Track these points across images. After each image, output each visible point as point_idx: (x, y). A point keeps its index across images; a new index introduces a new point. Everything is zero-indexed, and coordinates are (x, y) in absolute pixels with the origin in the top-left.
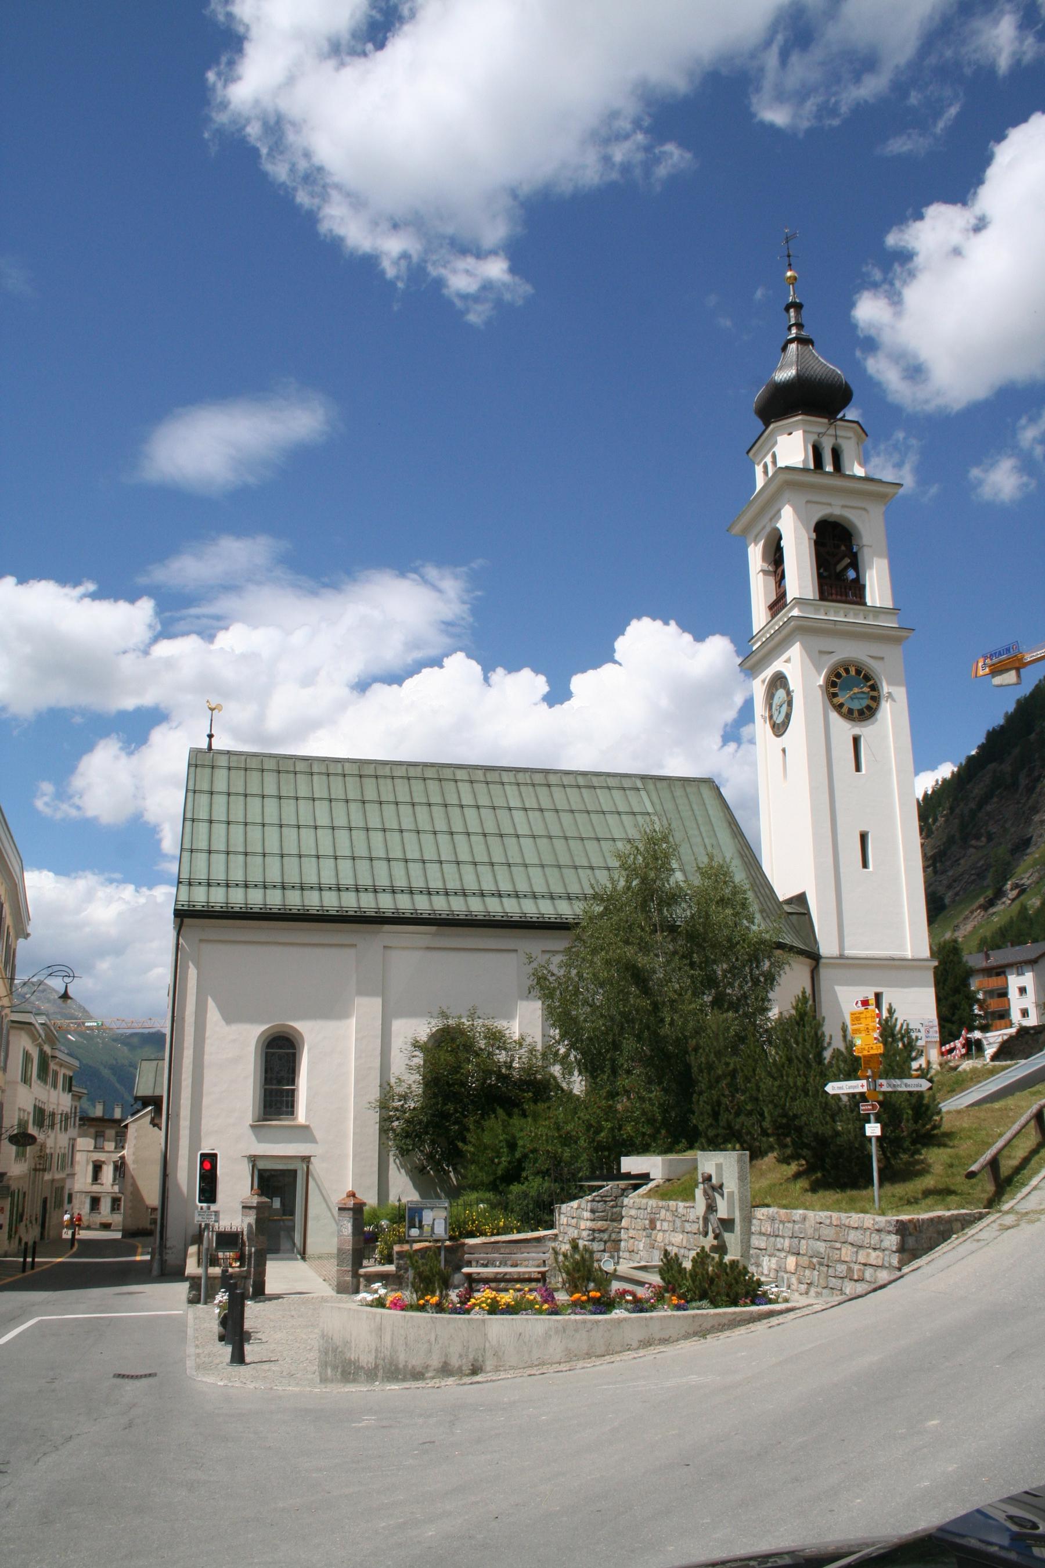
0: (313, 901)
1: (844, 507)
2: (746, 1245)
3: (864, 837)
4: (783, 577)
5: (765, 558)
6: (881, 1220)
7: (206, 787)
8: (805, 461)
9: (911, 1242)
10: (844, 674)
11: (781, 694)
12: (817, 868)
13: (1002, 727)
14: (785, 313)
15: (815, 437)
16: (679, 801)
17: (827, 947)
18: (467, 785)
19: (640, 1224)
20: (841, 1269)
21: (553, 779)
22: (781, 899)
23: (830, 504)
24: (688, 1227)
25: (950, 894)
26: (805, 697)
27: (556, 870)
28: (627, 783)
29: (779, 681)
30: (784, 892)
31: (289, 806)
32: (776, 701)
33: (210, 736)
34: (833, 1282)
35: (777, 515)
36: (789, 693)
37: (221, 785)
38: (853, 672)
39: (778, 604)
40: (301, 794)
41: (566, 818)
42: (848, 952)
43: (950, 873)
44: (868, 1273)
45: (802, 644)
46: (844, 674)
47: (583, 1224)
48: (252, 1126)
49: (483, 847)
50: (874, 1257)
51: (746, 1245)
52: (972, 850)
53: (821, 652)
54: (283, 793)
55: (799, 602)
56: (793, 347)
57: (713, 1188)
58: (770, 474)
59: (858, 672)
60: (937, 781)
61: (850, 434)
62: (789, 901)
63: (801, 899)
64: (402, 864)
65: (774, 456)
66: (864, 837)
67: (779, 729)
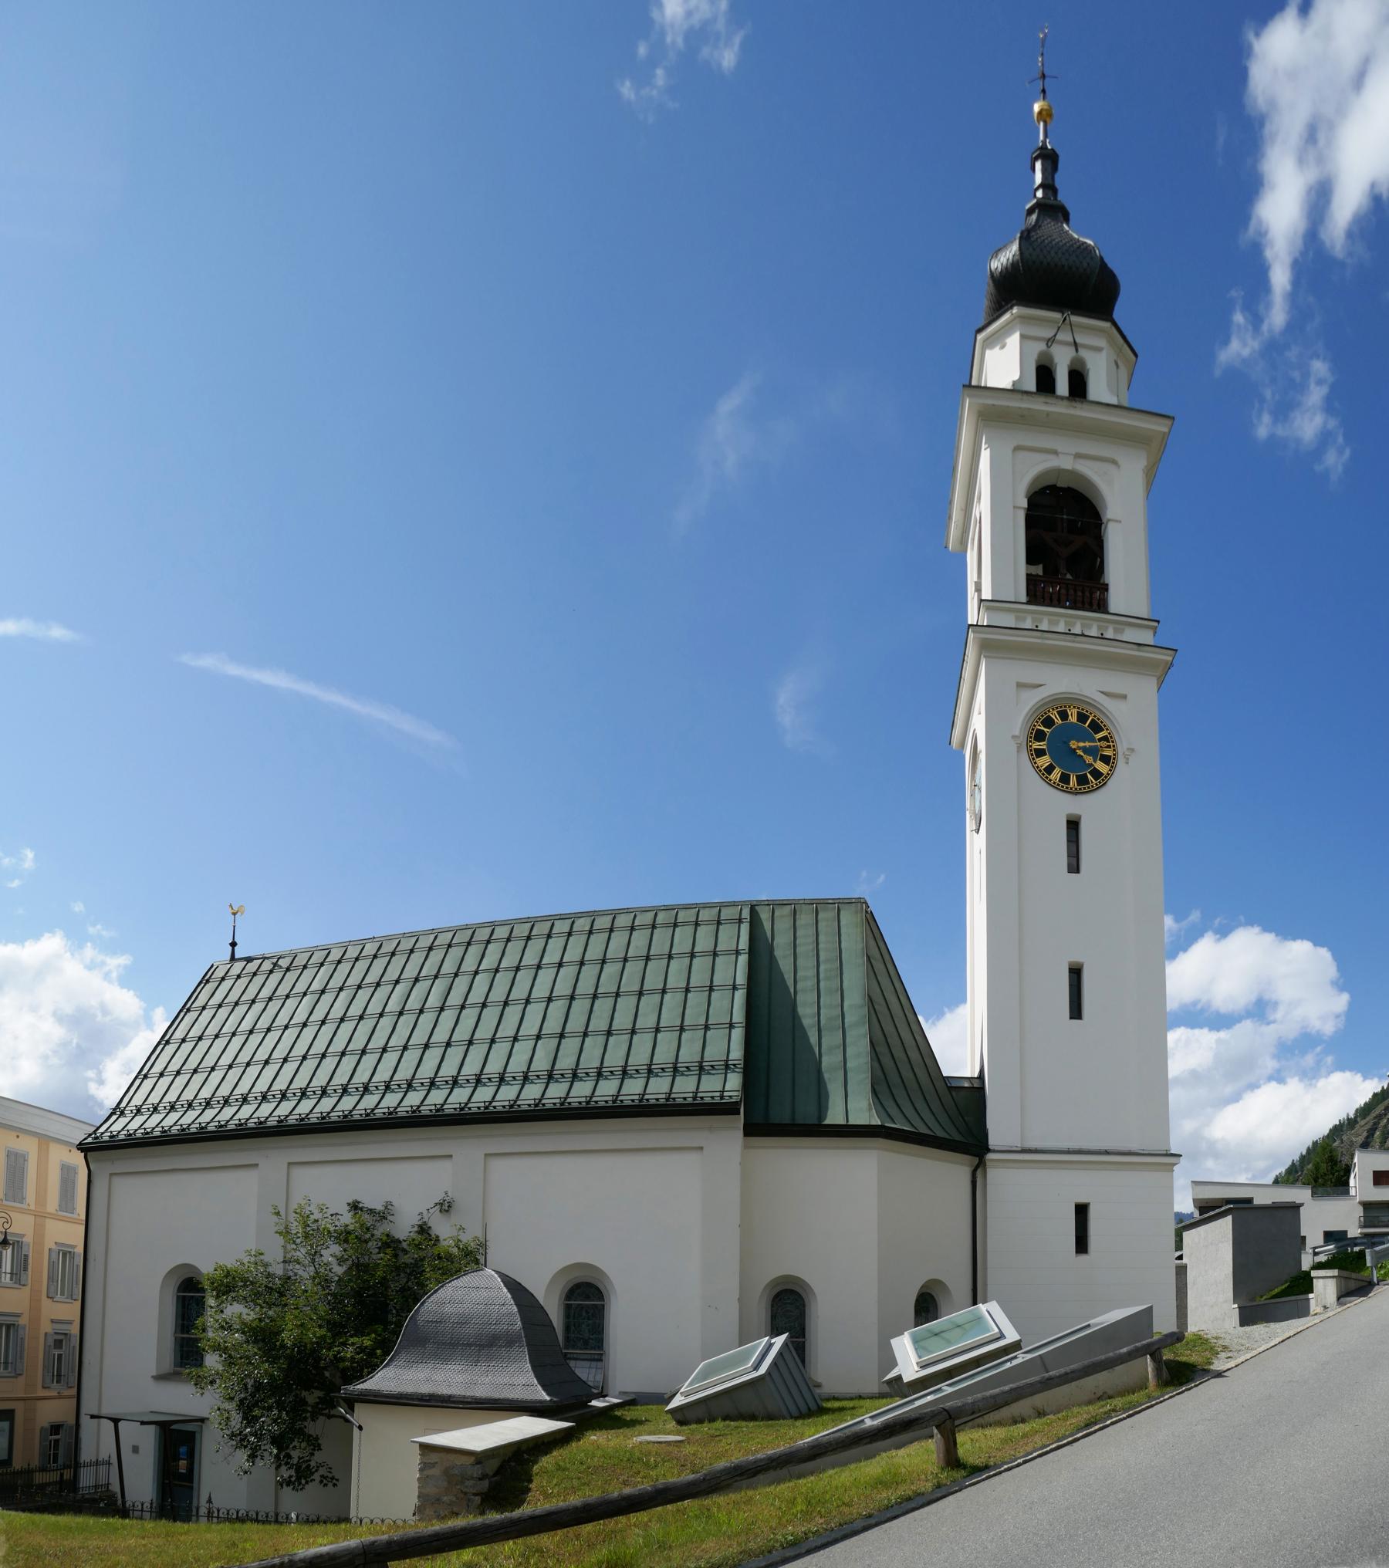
1: (1078, 456)
10: (1058, 721)
14: (982, 294)
15: (1042, 346)
23: (1056, 453)
33: (233, 944)
38: (1073, 718)
46: (1058, 721)
53: (1021, 686)
59: (1082, 717)
61: (1102, 342)
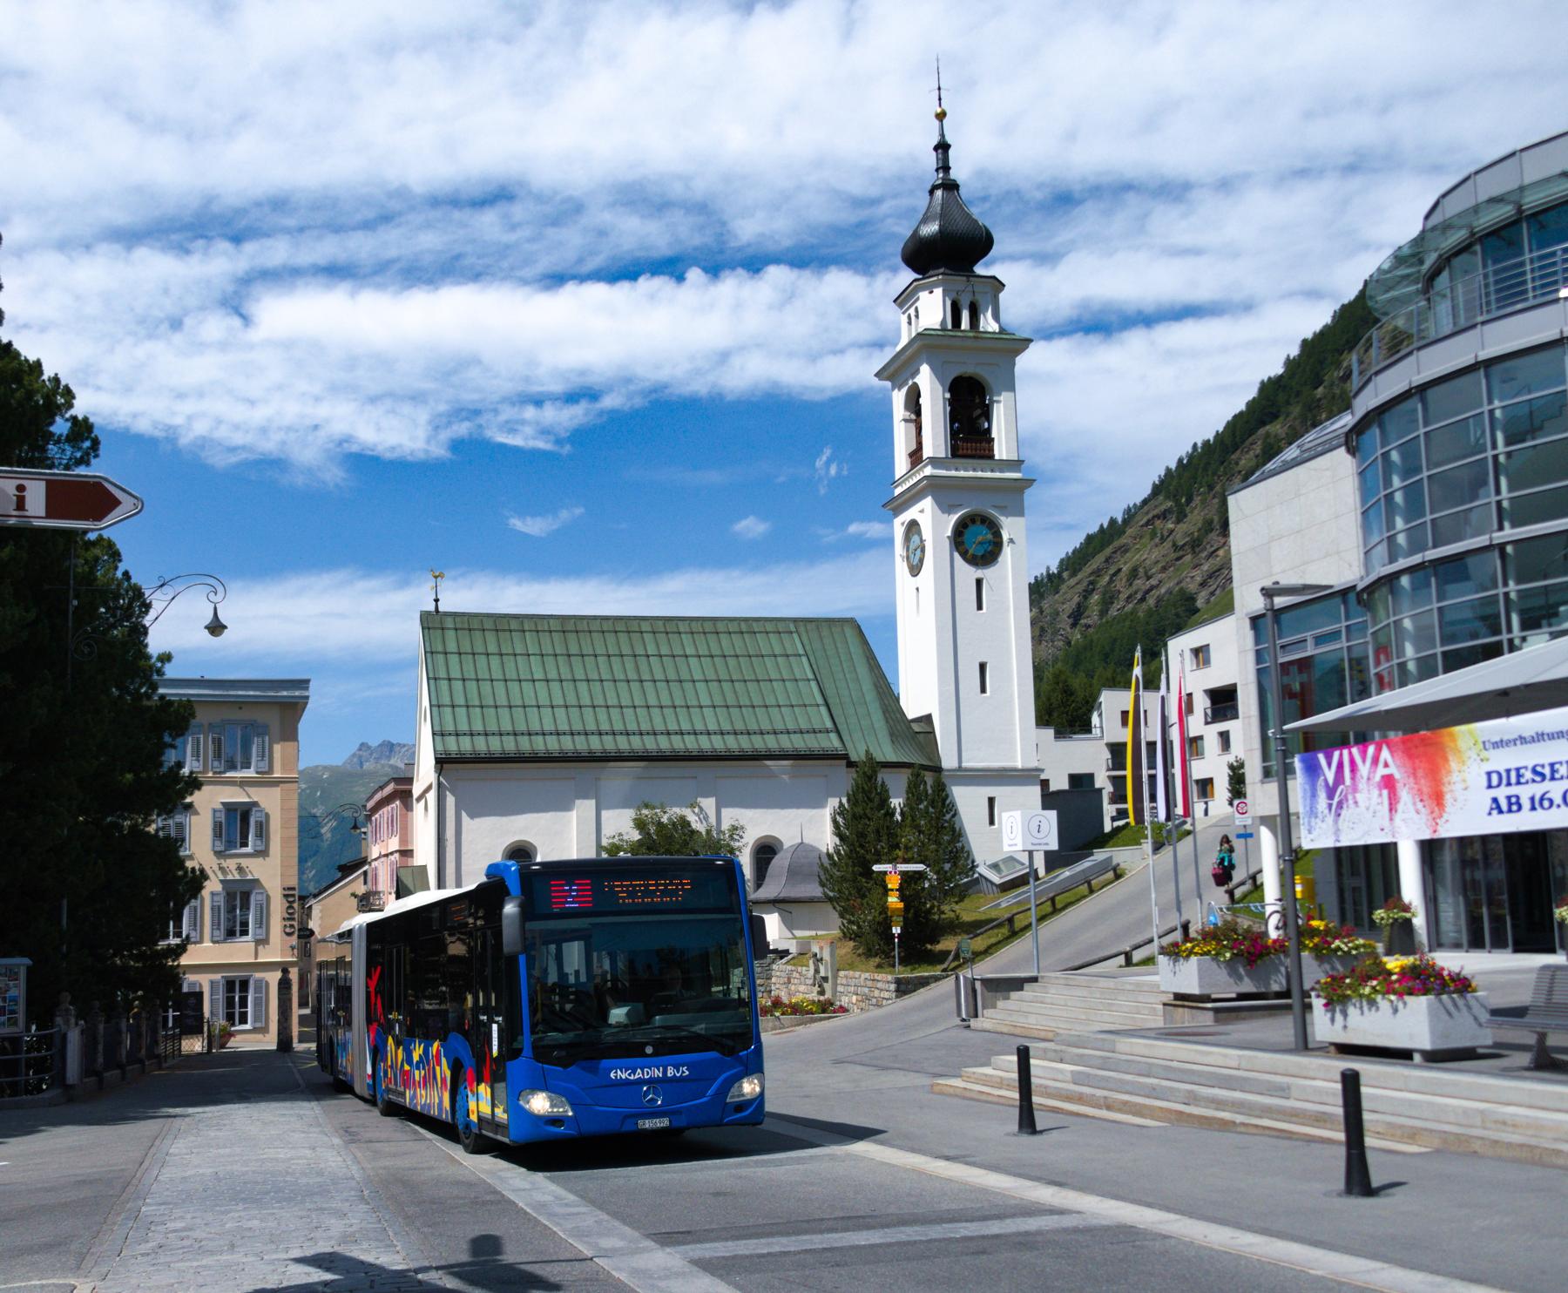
0: (539, 745)
2: (835, 991)
3: (983, 667)
6: (890, 978)
8: (944, 321)
9: (903, 987)
11: (915, 538)
13: (1280, 378)
16: (826, 641)
17: (948, 761)
21: (721, 627)
22: (910, 716)
28: (781, 627)
29: (913, 526)
30: (912, 712)
32: (912, 547)
35: (917, 372)
36: (922, 541)
37: (452, 647)
39: (916, 456)
40: (536, 677)
41: (732, 662)
42: (964, 765)
43: (1205, 567)
45: (935, 499)
51: (835, 991)
55: (934, 461)
56: (939, 193)
60: (1195, 445)
62: (918, 720)
63: (928, 719)
65: (916, 310)
66: (983, 667)
67: (915, 570)
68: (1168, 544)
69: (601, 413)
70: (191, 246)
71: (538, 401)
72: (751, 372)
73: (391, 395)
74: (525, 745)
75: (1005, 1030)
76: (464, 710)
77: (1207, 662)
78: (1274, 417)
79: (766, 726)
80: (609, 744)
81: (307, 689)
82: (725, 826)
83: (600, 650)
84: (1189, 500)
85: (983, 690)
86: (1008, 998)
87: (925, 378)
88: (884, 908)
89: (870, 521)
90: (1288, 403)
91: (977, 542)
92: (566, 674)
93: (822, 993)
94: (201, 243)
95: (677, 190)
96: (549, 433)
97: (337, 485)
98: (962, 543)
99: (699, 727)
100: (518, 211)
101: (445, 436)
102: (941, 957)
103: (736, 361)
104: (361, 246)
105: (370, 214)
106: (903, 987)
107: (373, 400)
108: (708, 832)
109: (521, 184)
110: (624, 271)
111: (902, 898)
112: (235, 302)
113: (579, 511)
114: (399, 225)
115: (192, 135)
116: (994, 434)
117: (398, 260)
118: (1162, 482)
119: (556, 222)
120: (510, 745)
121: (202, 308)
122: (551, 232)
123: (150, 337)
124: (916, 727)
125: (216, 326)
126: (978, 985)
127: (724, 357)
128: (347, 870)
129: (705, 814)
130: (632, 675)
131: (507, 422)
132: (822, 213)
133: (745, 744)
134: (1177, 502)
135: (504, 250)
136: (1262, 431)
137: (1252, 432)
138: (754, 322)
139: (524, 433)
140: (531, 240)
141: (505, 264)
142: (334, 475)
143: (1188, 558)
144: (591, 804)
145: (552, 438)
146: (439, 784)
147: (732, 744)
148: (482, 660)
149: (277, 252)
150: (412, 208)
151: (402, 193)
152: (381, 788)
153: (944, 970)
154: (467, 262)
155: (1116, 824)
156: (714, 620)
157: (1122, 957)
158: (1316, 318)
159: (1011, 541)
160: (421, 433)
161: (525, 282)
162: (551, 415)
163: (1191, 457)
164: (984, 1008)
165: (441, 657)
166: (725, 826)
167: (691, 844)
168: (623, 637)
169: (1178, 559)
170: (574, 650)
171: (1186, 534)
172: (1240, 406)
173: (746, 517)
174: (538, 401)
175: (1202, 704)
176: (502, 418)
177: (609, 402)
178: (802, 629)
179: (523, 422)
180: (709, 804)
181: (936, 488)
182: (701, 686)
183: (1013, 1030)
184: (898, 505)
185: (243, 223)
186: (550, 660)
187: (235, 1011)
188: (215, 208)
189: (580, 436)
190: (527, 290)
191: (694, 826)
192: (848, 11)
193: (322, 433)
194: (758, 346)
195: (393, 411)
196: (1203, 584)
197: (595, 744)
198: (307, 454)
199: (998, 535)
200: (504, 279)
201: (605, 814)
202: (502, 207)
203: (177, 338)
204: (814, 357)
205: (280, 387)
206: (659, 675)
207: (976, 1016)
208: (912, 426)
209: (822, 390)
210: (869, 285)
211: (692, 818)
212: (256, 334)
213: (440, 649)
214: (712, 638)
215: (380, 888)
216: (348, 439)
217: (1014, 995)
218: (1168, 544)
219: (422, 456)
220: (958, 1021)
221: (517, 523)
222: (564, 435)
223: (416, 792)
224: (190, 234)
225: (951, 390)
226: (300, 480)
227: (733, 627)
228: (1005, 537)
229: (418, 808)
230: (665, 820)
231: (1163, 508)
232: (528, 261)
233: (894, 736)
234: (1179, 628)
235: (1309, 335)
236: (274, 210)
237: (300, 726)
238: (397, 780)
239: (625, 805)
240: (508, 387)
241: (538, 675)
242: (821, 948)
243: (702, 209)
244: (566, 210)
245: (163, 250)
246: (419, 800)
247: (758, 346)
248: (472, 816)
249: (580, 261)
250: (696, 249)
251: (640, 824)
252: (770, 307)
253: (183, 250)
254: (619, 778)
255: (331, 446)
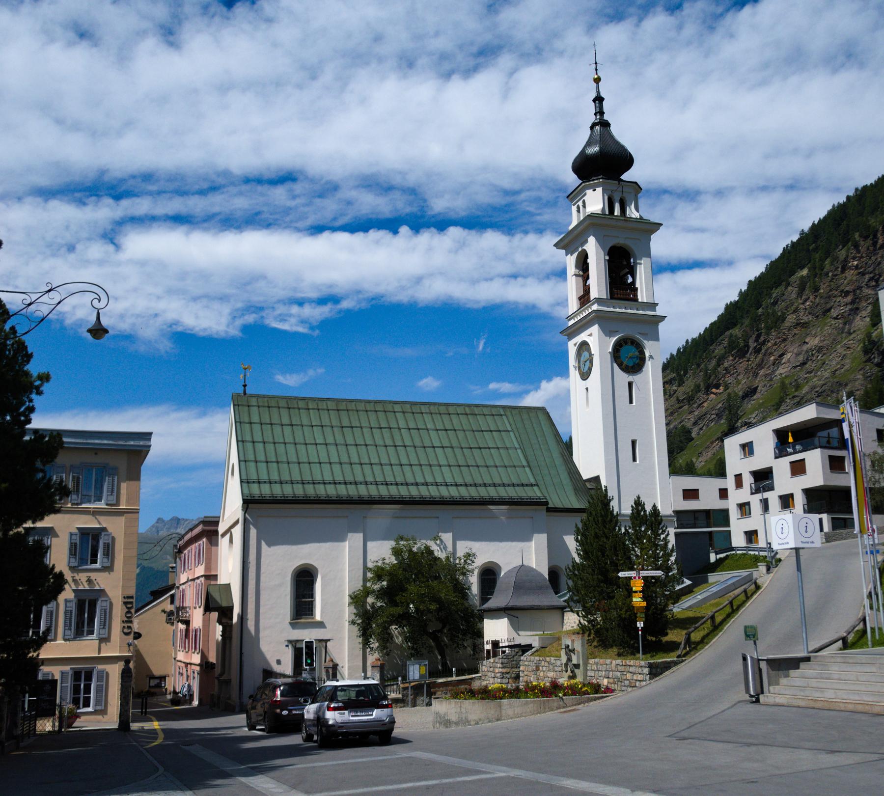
2: (585, 675)
3: (634, 443)
4: (588, 278)
5: (577, 267)
6: (643, 663)
7: (246, 419)
8: (603, 209)
9: (654, 671)
11: (585, 355)
12: (606, 462)
13: (736, 303)
18: (401, 414)
19: (530, 669)
20: (627, 683)
21: (451, 410)
24: (556, 669)
25: (696, 429)
26: (601, 359)
27: (457, 468)
31: (298, 431)
32: (582, 359)
33: (245, 386)
34: (623, 688)
36: (591, 355)
37: (255, 418)
39: (584, 299)
41: (461, 434)
43: (696, 413)
44: (638, 684)
45: (599, 325)
47: (497, 671)
48: (290, 623)
49: (414, 455)
50: (640, 677)
52: (713, 396)
54: (294, 423)
55: (598, 301)
57: (570, 651)
58: (582, 218)
63: (597, 479)
64: (369, 466)
65: (584, 202)
66: (634, 443)
67: (585, 376)
68: (674, 399)
69: (340, 311)
70: (87, 201)
71: (301, 303)
72: (435, 290)
73: (206, 296)
74: (310, 491)
75: (802, 704)
76: (264, 464)
77: (751, 453)
78: (734, 325)
79: (488, 480)
80: (373, 491)
81: (150, 440)
82: (460, 553)
83: (365, 424)
84: (686, 373)
85: (634, 460)
86: (787, 676)
87: (592, 246)
88: (631, 608)
89: (504, 381)
90: (742, 317)
91: (628, 357)
92: (339, 440)
93: (573, 677)
94: (94, 198)
95: (397, 180)
96: (306, 322)
97: (167, 352)
98: (619, 357)
99: (439, 480)
100: (298, 188)
101: (239, 322)
102: (672, 647)
103: (426, 282)
104: (196, 205)
105: (205, 185)
106: (654, 671)
107: (195, 299)
108: (448, 558)
109: (302, 172)
110: (360, 225)
111: (644, 598)
112: (111, 235)
113: (321, 371)
114: (223, 193)
115: (95, 133)
116: (638, 285)
117: (219, 213)
118: (668, 362)
119: (321, 196)
120: (299, 491)
121: (89, 239)
122: (318, 201)
123: (54, 255)
124: (588, 485)
125: (97, 250)
126: (763, 665)
127: (419, 280)
128: (157, 594)
129: (446, 545)
130: (389, 442)
131: (280, 315)
132: (484, 198)
133: (473, 493)
134: (678, 374)
135: (287, 211)
136: (728, 333)
137: (722, 333)
138: (439, 259)
139: (291, 322)
140: (304, 205)
141: (288, 219)
142: (165, 346)
143: (686, 407)
144: (359, 537)
145: (307, 325)
146: (245, 519)
147: (464, 492)
148: (277, 429)
149: (142, 206)
150: (233, 184)
151: (226, 173)
152: (191, 530)
153: (678, 657)
154: (263, 216)
155: (719, 556)
156: (447, 405)
157: (840, 642)
158: (756, 269)
159: (651, 357)
160: (224, 320)
161: (298, 230)
162: (308, 311)
163: (685, 348)
164: (769, 685)
165: (247, 426)
166: (460, 553)
167: (435, 567)
168: (381, 415)
169: (680, 408)
170: (345, 423)
171: (684, 393)
172: (714, 318)
173: (426, 377)
174: (301, 303)
175: (748, 480)
176: (278, 312)
177: (345, 305)
178: (509, 414)
179: (290, 315)
180: (447, 537)
181: (598, 318)
182: (439, 451)
183: (812, 704)
184: (572, 332)
185: (123, 188)
186: (328, 430)
187: (80, 697)
188: (106, 178)
189: (325, 324)
190: (299, 234)
191: (436, 554)
192: (507, 83)
193: (160, 320)
194: (441, 274)
195: (207, 307)
196: (695, 423)
197: (363, 491)
198: (149, 332)
199: (642, 353)
200: (285, 228)
201: (370, 544)
202: (289, 185)
203: (72, 257)
204: (474, 282)
205: (135, 290)
206: (408, 442)
207: (762, 693)
208: (580, 280)
209: (478, 302)
210: (510, 241)
211: (434, 547)
212: (123, 256)
213: (247, 420)
214: (446, 418)
215: (187, 604)
216: (177, 323)
217: (793, 673)
218: (674, 399)
219: (223, 335)
220: (747, 697)
221: (280, 378)
222: (315, 324)
223: (221, 529)
224: (88, 193)
225: (609, 254)
226: (142, 349)
227: (460, 410)
228: (647, 354)
229: (224, 542)
230: (415, 549)
231: (670, 377)
232: (303, 217)
233: (576, 490)
234: (732, 430)
235: (753, 279)
236: (143, 181)
237: (142, 468)
238: (204, 522)
239: (385, 538)
240: (282, 294)
241: (320, 440)
242: (573, 641)
243: (412, 191)
244: (328, 189)
245: (69, 202)
246: (223, 535)
247: (441, 274)
248: (269, 544)
249: (335, 219)
250: (407, 215)
251: (396, 552)
252: (450, 252)
253: (82, 203)
254: (381, 517)
255: (165, 327)
